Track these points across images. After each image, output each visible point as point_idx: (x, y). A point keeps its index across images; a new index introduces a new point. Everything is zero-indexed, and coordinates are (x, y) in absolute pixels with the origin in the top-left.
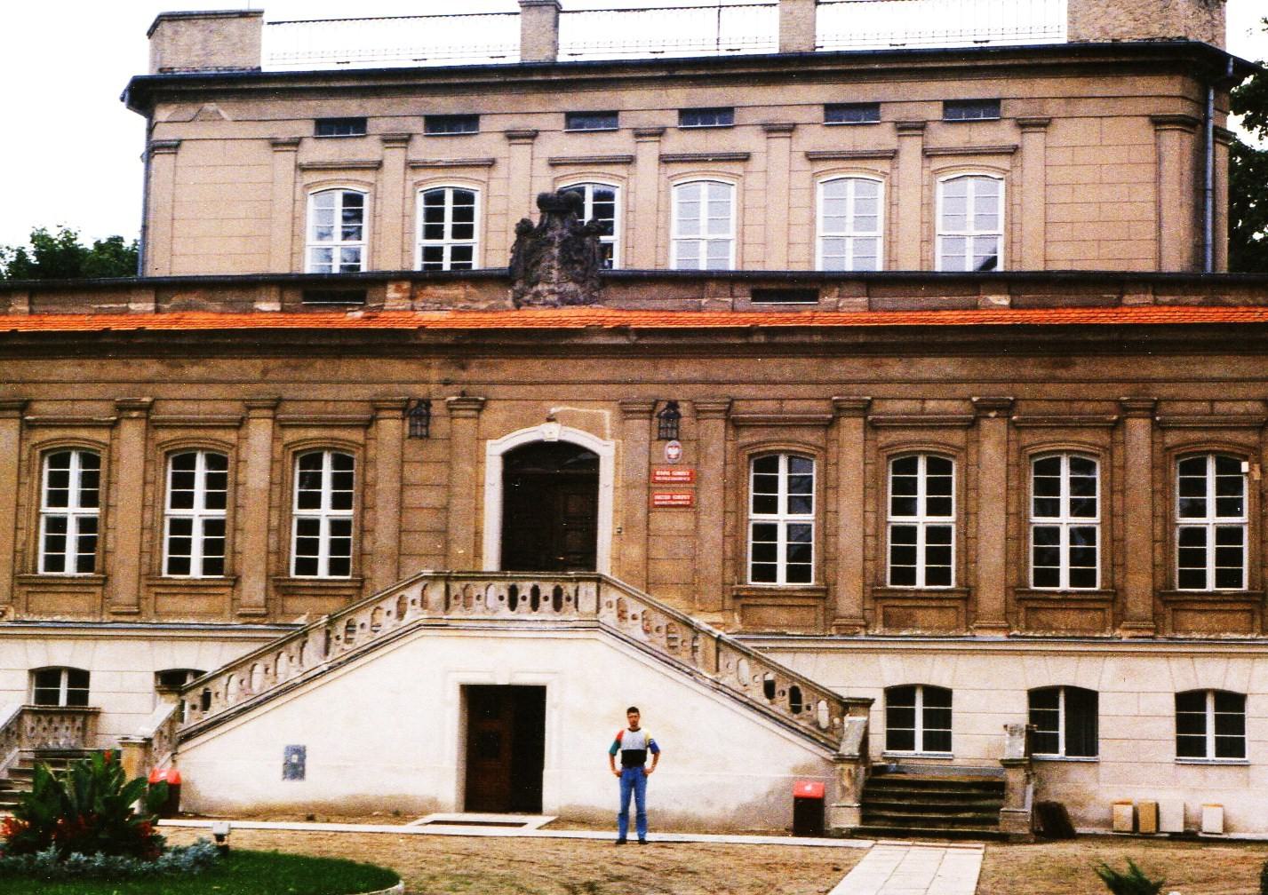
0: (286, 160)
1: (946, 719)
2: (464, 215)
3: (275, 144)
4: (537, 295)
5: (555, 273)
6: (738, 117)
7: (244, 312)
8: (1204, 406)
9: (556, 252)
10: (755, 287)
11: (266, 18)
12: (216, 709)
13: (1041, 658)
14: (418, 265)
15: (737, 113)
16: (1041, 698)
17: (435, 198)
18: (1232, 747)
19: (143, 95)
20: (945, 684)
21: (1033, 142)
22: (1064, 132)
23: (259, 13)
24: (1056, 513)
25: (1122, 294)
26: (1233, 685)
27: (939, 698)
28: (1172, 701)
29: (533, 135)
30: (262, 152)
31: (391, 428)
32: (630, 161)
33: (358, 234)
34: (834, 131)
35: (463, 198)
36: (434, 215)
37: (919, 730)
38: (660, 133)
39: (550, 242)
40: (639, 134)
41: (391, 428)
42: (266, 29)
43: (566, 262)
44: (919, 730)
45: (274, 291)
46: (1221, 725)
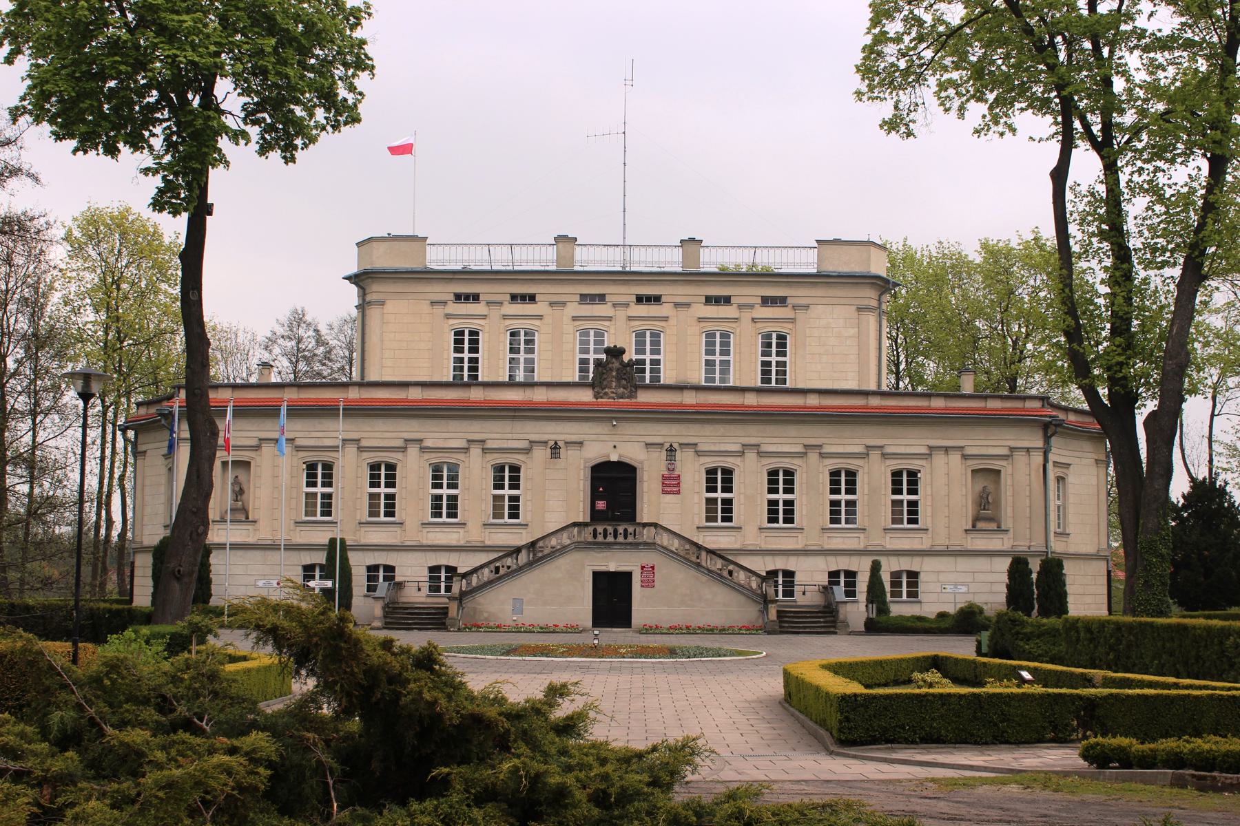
0: (439, 311)
2: (474, 343)
3: (433, 303)
4: (606, 394)
5: (614, 384)
6: (663, 299)
8: (742, 506)
9: (614, 374)
10: (634, 400)
11: (428, 242)
12: (492, 567)
17: (460, 333)
19: (355, 279)
21: (801, 315)
22: (816, 311)
23: (576, 239)
26: (915, 568)
28: (300, 568)
29: (564, 303)
30: (425, 307)
31: (541, 454)
32: (610, 318)
34: (709, 307)
35: (474, 333)
36: (458, 342)
39: (611, 370)
41: (541, 454)
42: (578, 249)
43: (619, 378)
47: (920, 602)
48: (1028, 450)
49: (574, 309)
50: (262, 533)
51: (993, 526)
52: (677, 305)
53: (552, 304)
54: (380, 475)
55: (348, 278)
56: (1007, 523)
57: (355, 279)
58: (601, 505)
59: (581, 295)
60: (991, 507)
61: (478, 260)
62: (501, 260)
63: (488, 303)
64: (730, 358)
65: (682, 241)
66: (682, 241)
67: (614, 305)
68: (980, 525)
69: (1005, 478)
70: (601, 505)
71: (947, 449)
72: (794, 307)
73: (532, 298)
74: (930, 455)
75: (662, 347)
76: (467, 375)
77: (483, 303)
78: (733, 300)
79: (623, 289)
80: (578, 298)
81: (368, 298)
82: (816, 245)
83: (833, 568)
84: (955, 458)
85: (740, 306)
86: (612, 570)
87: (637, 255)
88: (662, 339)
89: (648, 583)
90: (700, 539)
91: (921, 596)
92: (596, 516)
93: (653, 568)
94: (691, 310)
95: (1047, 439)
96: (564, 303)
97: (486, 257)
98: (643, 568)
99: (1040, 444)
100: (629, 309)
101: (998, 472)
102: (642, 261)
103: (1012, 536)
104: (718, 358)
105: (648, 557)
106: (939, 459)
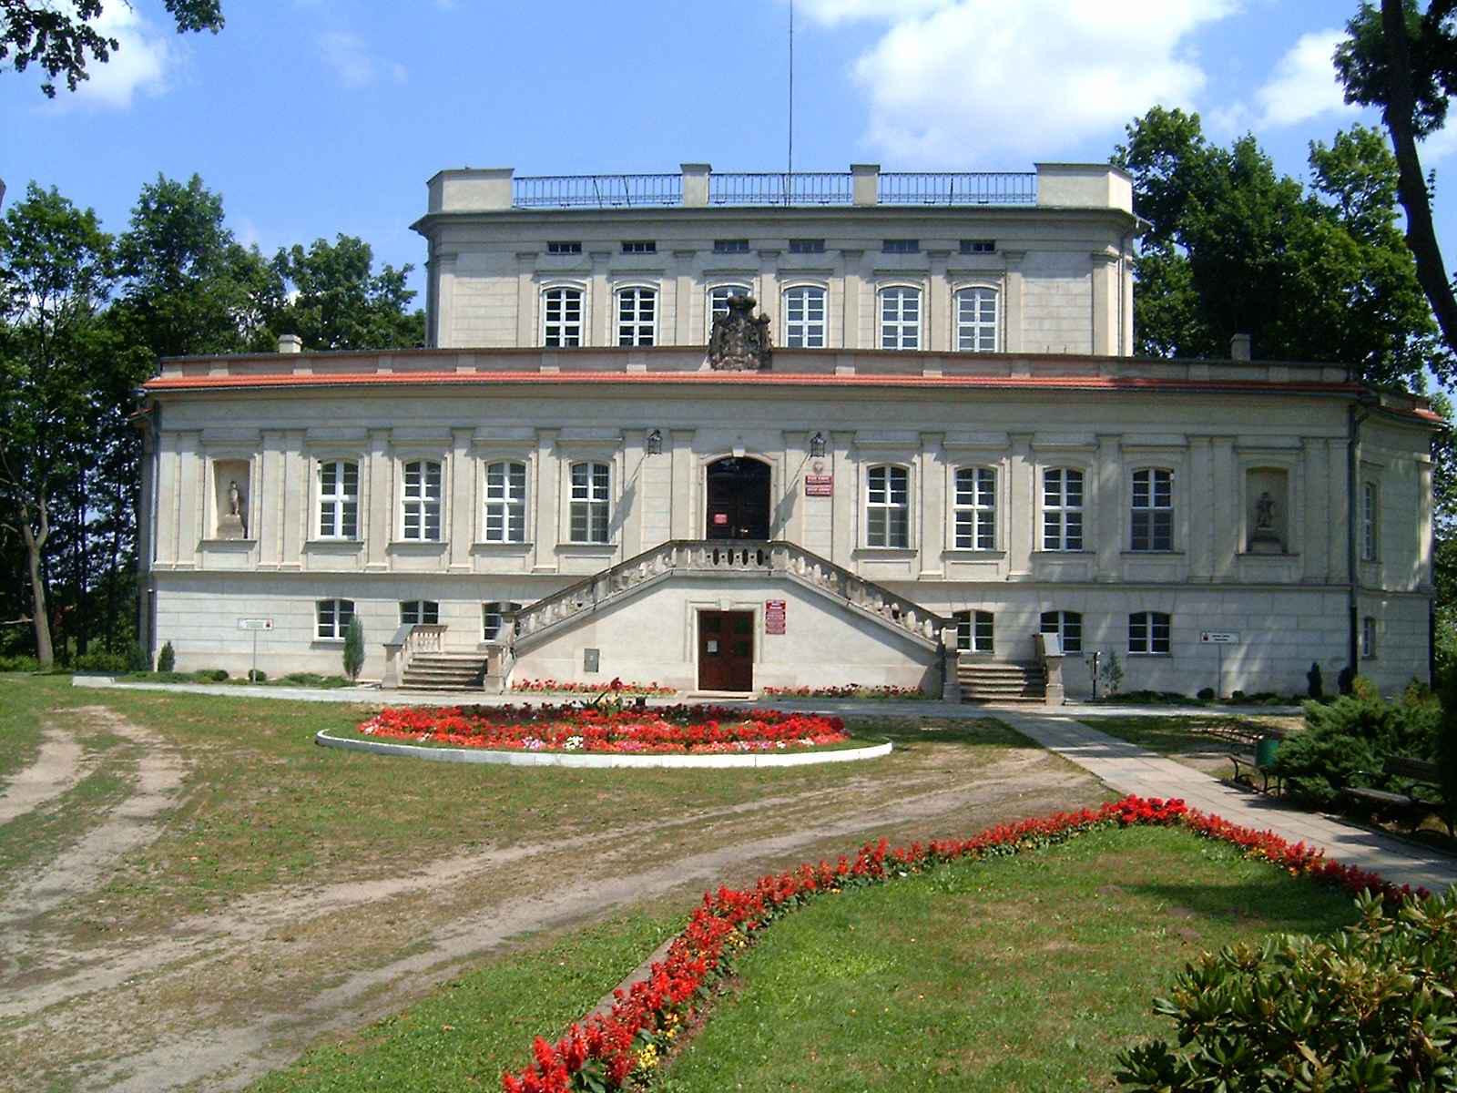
1: (1166, 632)
3: (519, 256)
7: (533, 371)
11: (515, 175)
13: (1121, 594)
14: (542, 343)
15: (826, 243)
16: (1138, 618)
18: (1162, 646)
20: (1076, 610)
24: (501, 496)
25: (923, 367)
26: (1166, 609)
27: (1163, 619)
28: (1127, 620)
29: (692, 252)
33: (991, 318)
37: (1150, 639)
38: (947, 253)
40: (931, 254)
44: (1150, 639)
45: (472, 359)
46: (1156, 632)
47: (1169, 656)
48: (1326, 440)
49: (708, 260)
50: (268, 558)
51: (1277, 548)
52: (844, 252)
53: (676, 253)
54: (1157, 491)
55: (413, 228)
56: (1295, 544)
57: (424, 227)
58: (721, 518)
59: (962, 242)
60: (1273, 522)
61: (581, 196)
62: (611, 195)
63: (760, 253)
64: (823, 323)
65: (852, 167)
66: (852, 167)
67: (760, 253)
68: (1259, 547)
69: (1295, 484)
70: (721, 518)
71: (1211, 438)
72: (1005, 254)
73: (651, 247)
74: (1188, 447)
75: (825, 310)
76: (553, 342)
77: (585, 255)
78: (922, 245)
79: (773, 232)
80: (712, 245)
81: (444, 249)
82: (1035, 170)
83: (1136, 610)
84: (1223, 453)
85: (931, 254)
86: (725, 608)
87: (798, 186)
88: (825, 299)
89: (777, 627)
90: (851, 568)
91: (1174, 648)
92: (715, 531)
93: (783, 605)
94: (866, 259)
95: (1354, 425)
96: (692, 252)
97: (623, 192)
98: (768, 605)
99: (1344, 431)
100: (950, 261)
101: (1284, 472)
102: (806, 194)
103: (1302, 564)
104: (977, 325)
105: (776, 595)
106: (1200, 457)
